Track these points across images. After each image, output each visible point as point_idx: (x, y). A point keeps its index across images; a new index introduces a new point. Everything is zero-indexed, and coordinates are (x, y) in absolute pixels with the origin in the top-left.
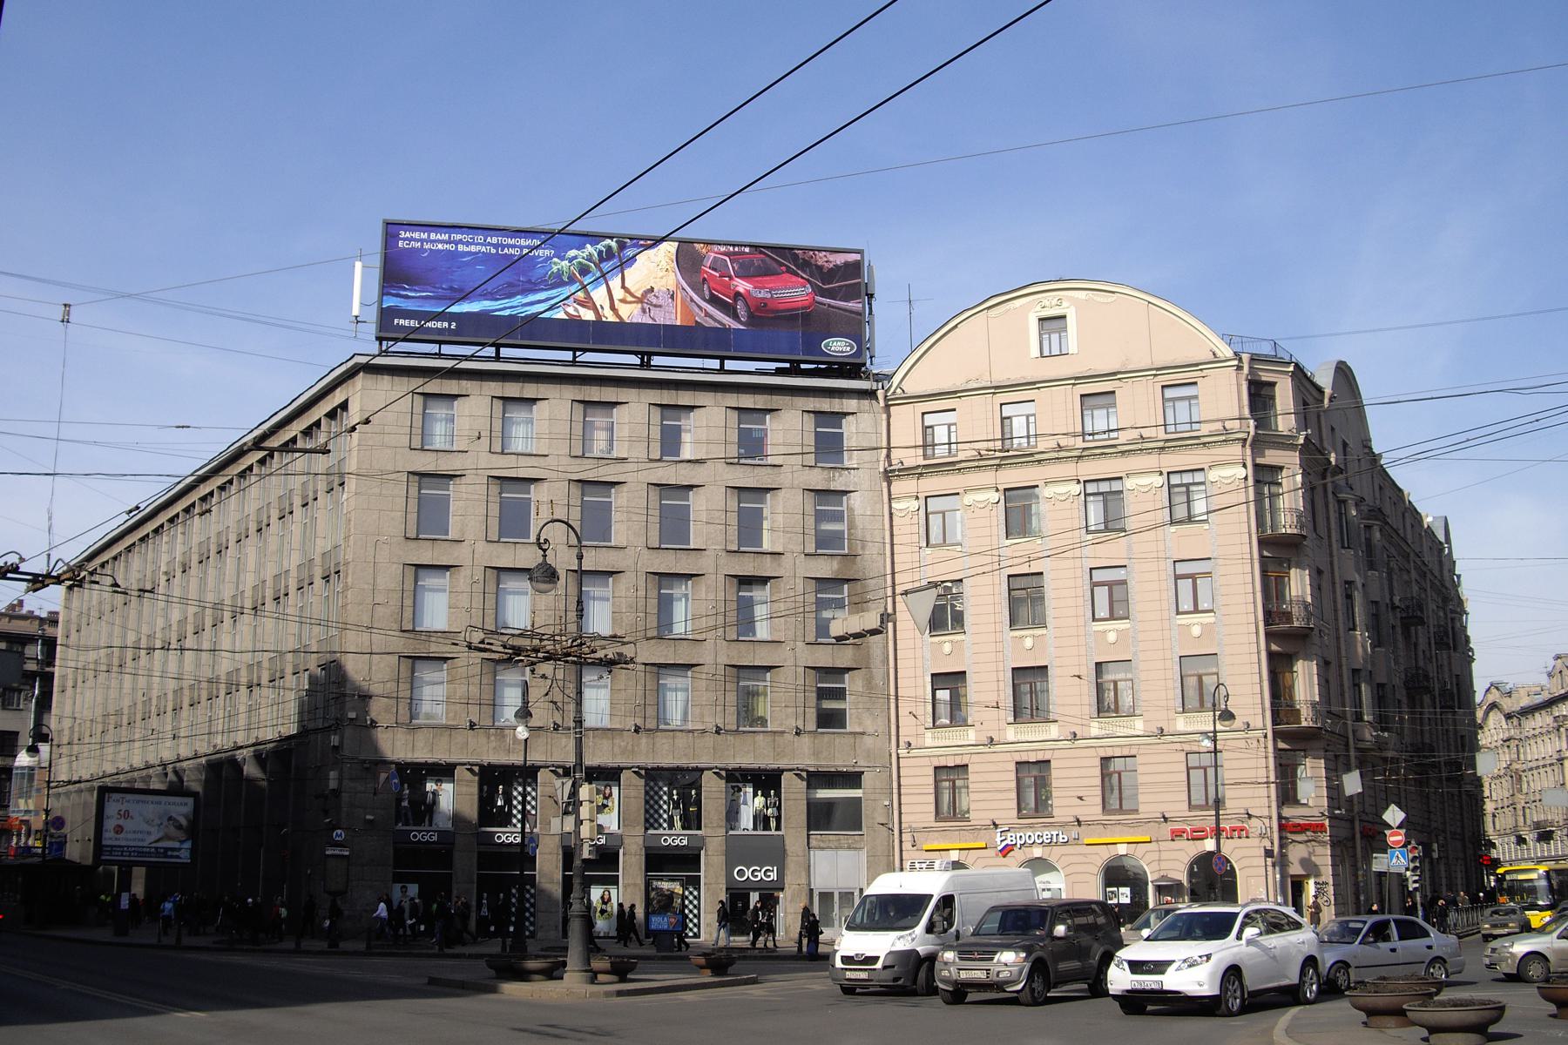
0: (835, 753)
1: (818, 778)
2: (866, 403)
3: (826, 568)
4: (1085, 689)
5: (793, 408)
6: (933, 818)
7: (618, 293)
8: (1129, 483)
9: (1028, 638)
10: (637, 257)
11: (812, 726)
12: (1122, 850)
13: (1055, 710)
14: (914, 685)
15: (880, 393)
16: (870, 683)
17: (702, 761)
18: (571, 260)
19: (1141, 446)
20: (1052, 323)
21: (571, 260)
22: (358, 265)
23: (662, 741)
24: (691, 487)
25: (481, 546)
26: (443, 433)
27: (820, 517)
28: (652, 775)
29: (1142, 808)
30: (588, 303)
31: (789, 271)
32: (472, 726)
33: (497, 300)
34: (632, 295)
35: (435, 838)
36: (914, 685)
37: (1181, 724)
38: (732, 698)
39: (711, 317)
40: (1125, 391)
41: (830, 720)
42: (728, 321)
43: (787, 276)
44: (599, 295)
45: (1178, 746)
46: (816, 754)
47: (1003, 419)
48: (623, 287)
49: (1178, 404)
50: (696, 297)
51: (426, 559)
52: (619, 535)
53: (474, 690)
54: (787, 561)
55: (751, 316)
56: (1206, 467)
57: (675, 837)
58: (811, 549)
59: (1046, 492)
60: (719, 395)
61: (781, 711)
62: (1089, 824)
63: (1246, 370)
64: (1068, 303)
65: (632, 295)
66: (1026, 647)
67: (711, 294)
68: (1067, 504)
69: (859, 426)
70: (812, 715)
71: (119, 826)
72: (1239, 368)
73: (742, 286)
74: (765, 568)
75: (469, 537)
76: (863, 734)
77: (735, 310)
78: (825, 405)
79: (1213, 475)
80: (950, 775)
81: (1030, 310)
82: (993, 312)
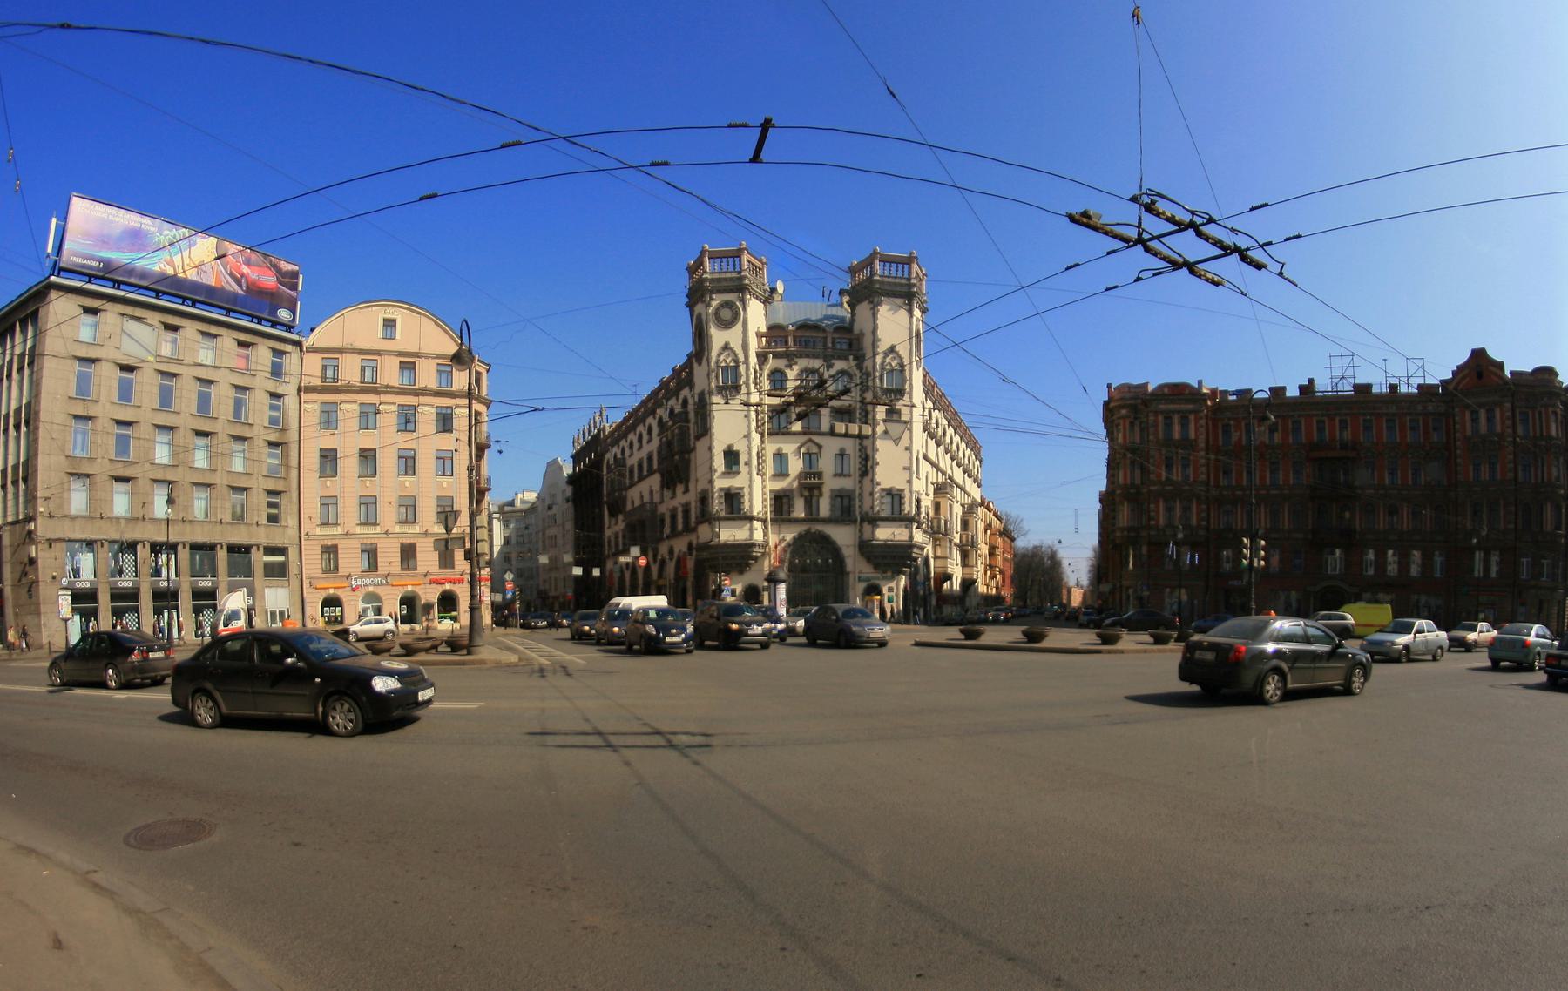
1: (270, 550)
3: (273, 437)
5: (264, 344)
7: (187, 261)
12: (410, 588)
18: (165, 236)
20: (390, 324)
21: (165, 236)
28: (195, 547)
30: (171, 263)
31: (267, 267)
33: (125, 252)
34: (193, 263)
35: (131, 585)
36: (311, 507)
39: (230, 285)
42: (236, 287)
43: (266, 269)
44: (177, 260)
46: (267, 537)
48: (189, 257)
50: (223, 271)
55: (247, 287)
57: (205, 583)
58: (267, 424)
60: (230, 331)
62: (394, 575)
64: (400, 315)
65: (193, 263)
67: (231, 272)
69: (292, 361)
71: (174, 595)
73: (245, 269)
74: (246, 433)
75: (222, 417)
77: (241, 282)
78: (278, 345)
80: (331, 551)
81: (379, 313)
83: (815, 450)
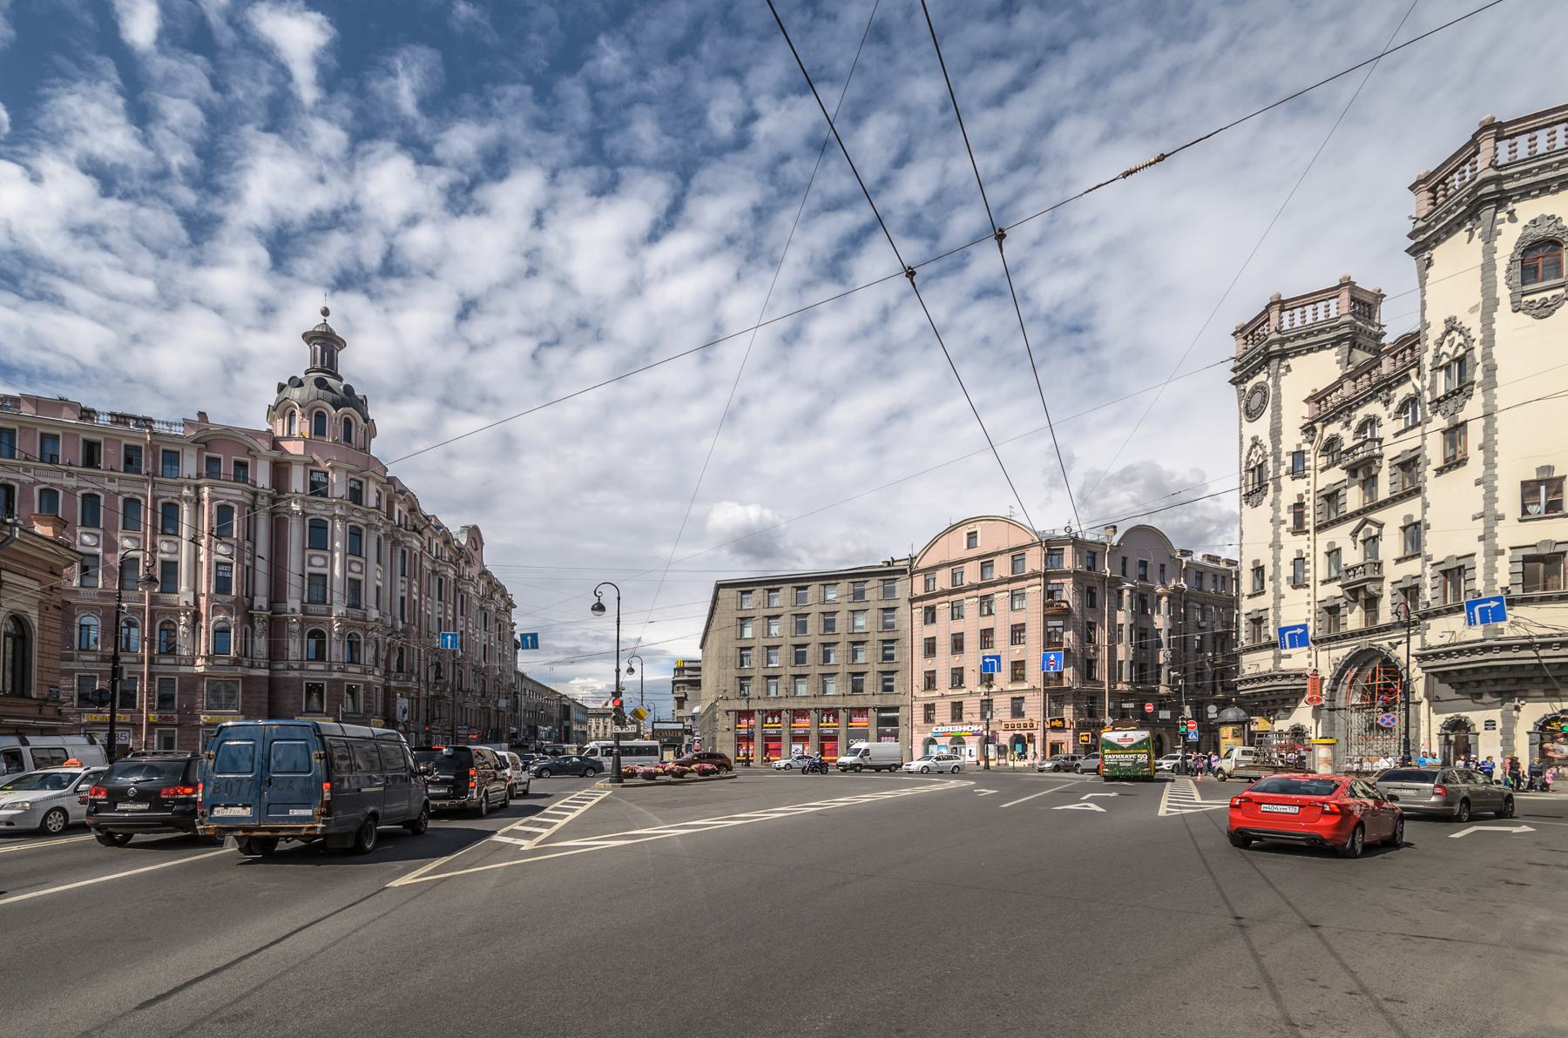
0: (889, 701)
1: (881, 710)
9: (1018, 648)
10: (1338, 283)
11: (879, 692)
14: (919, 680)
17: (869, 704)
19: (1002, 581)
22: (247, 812)
23: (824, 700)
25: (761, 639)
27: (885, 618)
32: (759, 698)
37: (979, 690)
38: (850, 683)
40: (997, 560)
41: (889, 689)
51: (743, 646)
52: (809, 630)
53: (760, 686)
54: (871, 635)
59: (966, 602)
70: (880, 687)
83: (1375, 531)
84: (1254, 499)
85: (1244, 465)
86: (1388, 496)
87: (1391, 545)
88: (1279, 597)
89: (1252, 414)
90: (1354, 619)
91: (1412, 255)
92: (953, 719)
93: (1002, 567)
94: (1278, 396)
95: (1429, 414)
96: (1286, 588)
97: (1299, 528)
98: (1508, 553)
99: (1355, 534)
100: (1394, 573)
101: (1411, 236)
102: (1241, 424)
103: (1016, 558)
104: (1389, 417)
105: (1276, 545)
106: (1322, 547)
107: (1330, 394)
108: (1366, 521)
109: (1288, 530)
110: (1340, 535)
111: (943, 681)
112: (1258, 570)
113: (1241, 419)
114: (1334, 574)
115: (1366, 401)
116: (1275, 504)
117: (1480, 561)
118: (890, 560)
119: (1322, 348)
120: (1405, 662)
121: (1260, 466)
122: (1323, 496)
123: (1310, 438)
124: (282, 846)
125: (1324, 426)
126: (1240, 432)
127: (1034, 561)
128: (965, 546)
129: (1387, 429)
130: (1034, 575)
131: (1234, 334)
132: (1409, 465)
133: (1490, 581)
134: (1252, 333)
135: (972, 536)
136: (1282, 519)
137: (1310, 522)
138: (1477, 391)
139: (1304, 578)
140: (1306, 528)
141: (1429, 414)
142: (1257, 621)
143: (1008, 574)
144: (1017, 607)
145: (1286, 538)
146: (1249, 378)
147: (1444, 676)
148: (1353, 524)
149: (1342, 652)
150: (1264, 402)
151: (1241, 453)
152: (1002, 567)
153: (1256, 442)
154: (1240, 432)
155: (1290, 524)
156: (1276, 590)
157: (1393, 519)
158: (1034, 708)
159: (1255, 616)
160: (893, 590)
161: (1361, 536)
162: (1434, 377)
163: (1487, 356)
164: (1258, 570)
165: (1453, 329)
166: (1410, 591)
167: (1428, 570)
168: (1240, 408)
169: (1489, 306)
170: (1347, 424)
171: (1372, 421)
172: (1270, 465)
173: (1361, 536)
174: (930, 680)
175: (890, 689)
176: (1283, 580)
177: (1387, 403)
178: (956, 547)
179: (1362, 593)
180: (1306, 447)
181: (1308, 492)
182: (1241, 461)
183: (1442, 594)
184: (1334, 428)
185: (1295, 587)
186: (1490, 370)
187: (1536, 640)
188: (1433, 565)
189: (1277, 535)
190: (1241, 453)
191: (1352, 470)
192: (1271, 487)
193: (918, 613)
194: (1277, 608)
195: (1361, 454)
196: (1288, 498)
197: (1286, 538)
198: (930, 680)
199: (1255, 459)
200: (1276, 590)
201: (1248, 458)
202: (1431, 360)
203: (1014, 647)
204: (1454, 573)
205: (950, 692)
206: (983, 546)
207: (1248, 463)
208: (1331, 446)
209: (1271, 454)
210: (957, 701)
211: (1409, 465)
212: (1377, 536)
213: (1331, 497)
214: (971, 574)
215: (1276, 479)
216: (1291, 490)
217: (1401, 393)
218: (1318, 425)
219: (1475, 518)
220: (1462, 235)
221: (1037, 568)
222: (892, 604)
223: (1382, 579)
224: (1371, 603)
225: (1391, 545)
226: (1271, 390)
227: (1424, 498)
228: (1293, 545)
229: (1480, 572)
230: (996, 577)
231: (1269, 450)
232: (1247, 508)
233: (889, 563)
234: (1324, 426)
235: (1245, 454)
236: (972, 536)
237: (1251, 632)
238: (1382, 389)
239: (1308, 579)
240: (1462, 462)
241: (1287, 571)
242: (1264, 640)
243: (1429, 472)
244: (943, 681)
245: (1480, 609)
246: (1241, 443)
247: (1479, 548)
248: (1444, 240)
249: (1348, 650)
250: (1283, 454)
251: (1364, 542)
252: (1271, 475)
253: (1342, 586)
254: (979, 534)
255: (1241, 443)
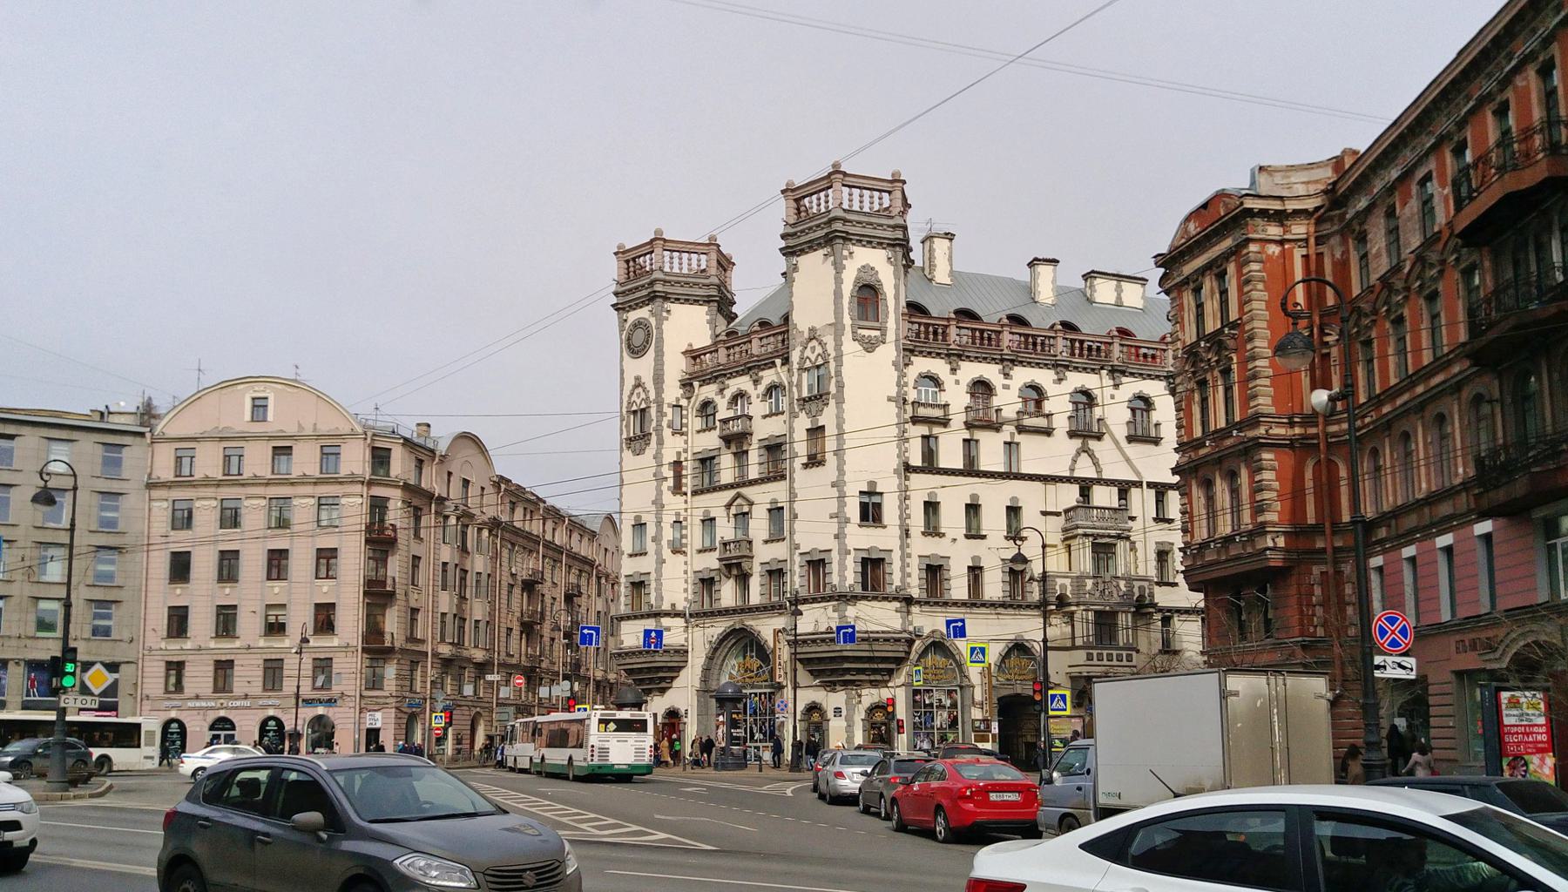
2: (138, 439)
4: (258, 620)
6: (260, 689)
8: (295, 502)
9: (277, 586)
13: (239, 631)
14: (159, 620)
15: (148, 435)
16: (1062, 601)
19: (303, 481)
24: (11, 486)
26: (379, 418)
29: (235, 690)
45: (160, 658)
47: (225, 456)
49: (330, 457)
56: (243, 497)
61: (44, 625)
63: (369, 441)
66: (227, 595)
68: (208, 512)
72: (366, 439)
76: (121, 641)
79: (343, 501)
82: (224, 391)
83: (746, 509)
84: (637, 445)
85: (625, 404)
86: (757, 476)
87: (759, 526)
88: (661, 562)
89: (636, 351)
90: (728, 594)
91: (784, 255)
92: (216, 690)
93: (305, 460)
94: (660, 340)
95: (797, 410)
96: (666, 553)
97: (677, 489)
98: (853, 552)
99: (728, 506)
100: (764, 554)
101: (783, 237)
102: (622, 356)
103: (326, 450)
104: (758, 397)
105: (659, 504)
106: (699, 515)
107: (705, 354)
108: (738, 496)
109: (669, 488)
110: (716, 503)
111: (202, 624)
112: (639, 526)
113: (622, 352)
114: (707, 544)
115: (739, 374)
116: (658, 456)
117: (835, 556)
118: (103, 409)
119: (696, 302)
120: (772, 646)
121: (643, 411)
122: (700, 459)
123: (687, 395)
124: (872, 809)
125: (700, 386)
126: (621, 365)
127: (355, 459)
128: (248, 416)
129: (757, 408)
130: (352, 480)
131: (616, 254)
132: (774, 449)
133: (843, 578)
134: (634, 259)
135: (259, 406)
136: (665, 475)
137: (689, 483)
138: (832, 402)
139: (681, 544)
140: (684, 489)
141: (797, 410)
142: (638, 585)
143: (314, 470)
144: (324, 523)
145: (668, 497)
146: (632, 308)
147: (806, 662)
148: (728, 495)
149: (718, 628)
150: (647, 341)
151: (622, 390)
152: (305, 460)
153: (638, 384)
154: (621, 365)
155: (670, 482)
156: (659, 553)
157: (762, 496)
158: (349, 670)
159: (637, 580)
160: (117, 463)
161: (733, 510)
162: (800, 375)
163: (838, 373)
164: (639, 526)
165: (814, 338)
166: (776, 573)
167: (797, 559)
168: (621, 339)
169: (837, 328)
170: (722, 391)
171: (740, 396)
172: (653, 411)
173: (733, 510)
174: (178, 621)
175: (106, 632)
176: (664, 543)
177: (756, 382)
178: (239, 417)
179: (736, 569)
180: (684, 402)
181: (686, 451)
182: (621, 399)
183: (807, 584)
184: (709, 392)
185: (675, 552)
186: (840, 386)
187: (871, 635)
188: (801, 554)
189: (659, 493)
190: (622, 390)
191: (728, 440)
192: (654, 438)
193: (161, 511)
194: (659, 571)
195: (736, 427)
196: (669, 456)
197: (668, 497)
198: (178, 621)
199: (638, 402)
200: (659, 553)
201: (630, 397)
202: (798, 360)
203: (270, 583)
204: (817, 565)
205: (212, 644)
206: (277, 420)
207: (630, 404)
208: (706, 408)
209: (655, 401)
210: (224, 658)
211: (774, 449)
212: (747, 513)
213: (706, 462)
214: (257, 461)
215: (659, 430)
216: (672, 447)
217: (768, 376)
218: (696, 384)
219: (831, 517)
220: (821, 252)
221: (358, 471)
222: (115, 486)
223: (752, 557)
224: (743, 579)
225: (759, 526)
226: (655, 331)
227: (791, 488)
228: (674, 503)
229: (835, 567)
230: (296, 473)
231: (652, 396)
232: (628, 454)
233: (102, 414)
234: (700, 386)
235: (626, 393)
236: (259, 406)
237: (630, 598)
238: (752, 368)
239: (686, 545)
240: (821, 463)
241: (668, 534)
242: (645, 609)
243: (798, 463)
244: (202, 624)
245: (60, 523)
246: (622, 379)
247: (832, 544)
248: (807, 253)
249: (722, 630)
250: (665, 406)
251: (735, 515)
252: (654, 424)
253: (720, 560)
254: (271, 404)
255: (622, 379)
